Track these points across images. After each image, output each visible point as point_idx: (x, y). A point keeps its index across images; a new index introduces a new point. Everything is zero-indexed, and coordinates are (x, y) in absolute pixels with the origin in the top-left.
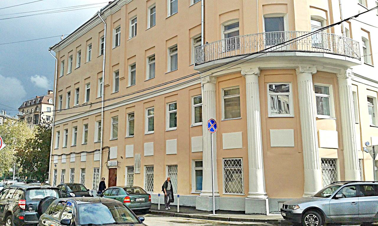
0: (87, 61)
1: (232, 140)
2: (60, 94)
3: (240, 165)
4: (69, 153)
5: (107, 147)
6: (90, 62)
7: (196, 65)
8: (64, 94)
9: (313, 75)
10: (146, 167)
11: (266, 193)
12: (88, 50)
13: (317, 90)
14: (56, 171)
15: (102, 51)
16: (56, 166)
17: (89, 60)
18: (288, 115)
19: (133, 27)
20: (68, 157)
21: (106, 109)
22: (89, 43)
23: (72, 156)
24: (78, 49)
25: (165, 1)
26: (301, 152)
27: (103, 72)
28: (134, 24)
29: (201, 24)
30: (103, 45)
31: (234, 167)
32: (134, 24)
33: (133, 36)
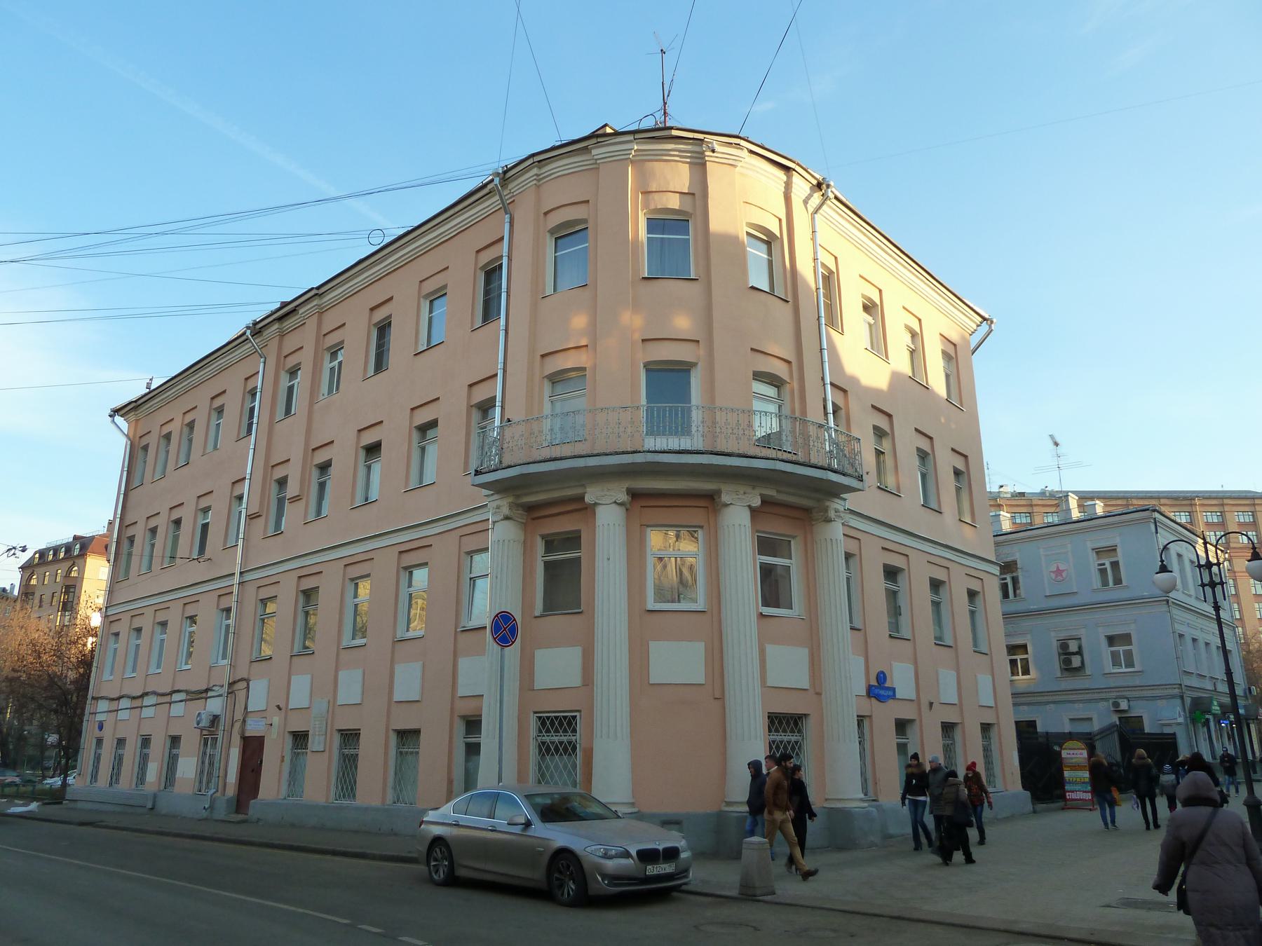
0: (210, 447)
1: (557, 667)
2: (130, 532)
3: (574, 731)
4: (168, 691)
5: (242, 680)
6: (216, 452)
7: (477, 473)
8: (139, 532)
9: (754, 511)
10: (540, 718)
11: (631, 801)
12: (214, 422)
13: (766, 545)
14: (99, 741)
15: (250, 425)
16: (101, 728)
17: (215, 448)
18: (693, 607)
19: (332, 369)
20: (137, 703)
21: (248, 577)
22: (217, 403)
23: (148, 701)
24: (188, 418)
25: (4, 266)
26: (721, 699)
27: (247, 482)
28: (336, 363)
29: (496, 375)
30: (252, 410)
31: (559, 732)
32: (336, 363)
33: (330, 391)
